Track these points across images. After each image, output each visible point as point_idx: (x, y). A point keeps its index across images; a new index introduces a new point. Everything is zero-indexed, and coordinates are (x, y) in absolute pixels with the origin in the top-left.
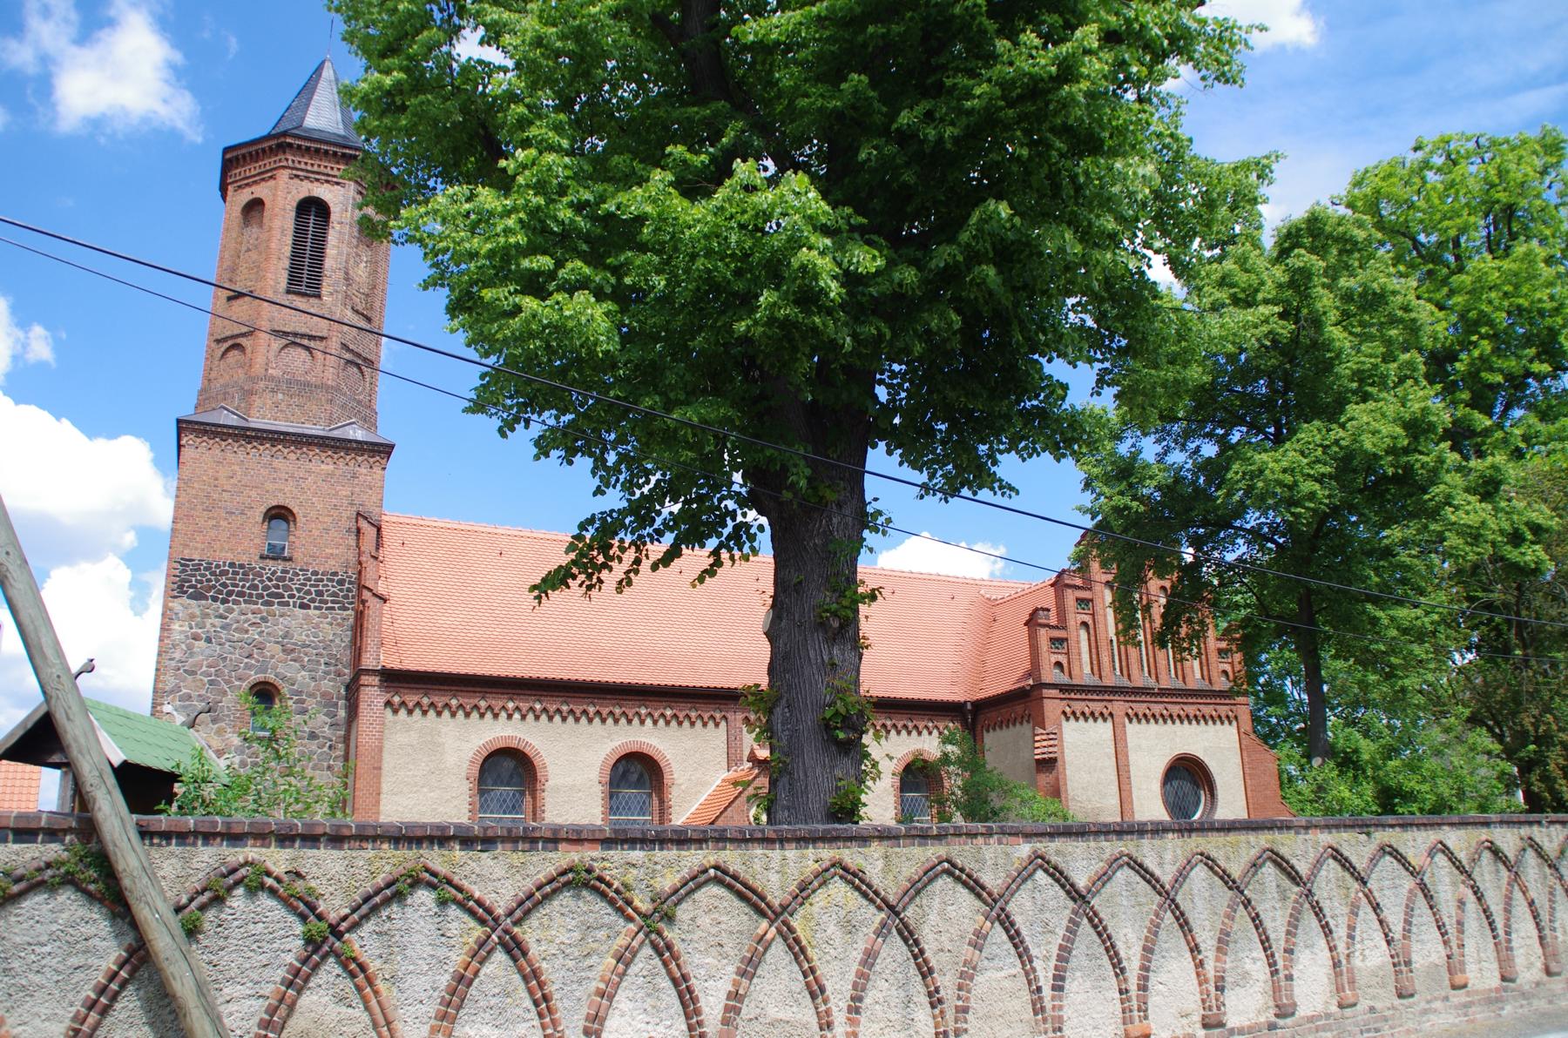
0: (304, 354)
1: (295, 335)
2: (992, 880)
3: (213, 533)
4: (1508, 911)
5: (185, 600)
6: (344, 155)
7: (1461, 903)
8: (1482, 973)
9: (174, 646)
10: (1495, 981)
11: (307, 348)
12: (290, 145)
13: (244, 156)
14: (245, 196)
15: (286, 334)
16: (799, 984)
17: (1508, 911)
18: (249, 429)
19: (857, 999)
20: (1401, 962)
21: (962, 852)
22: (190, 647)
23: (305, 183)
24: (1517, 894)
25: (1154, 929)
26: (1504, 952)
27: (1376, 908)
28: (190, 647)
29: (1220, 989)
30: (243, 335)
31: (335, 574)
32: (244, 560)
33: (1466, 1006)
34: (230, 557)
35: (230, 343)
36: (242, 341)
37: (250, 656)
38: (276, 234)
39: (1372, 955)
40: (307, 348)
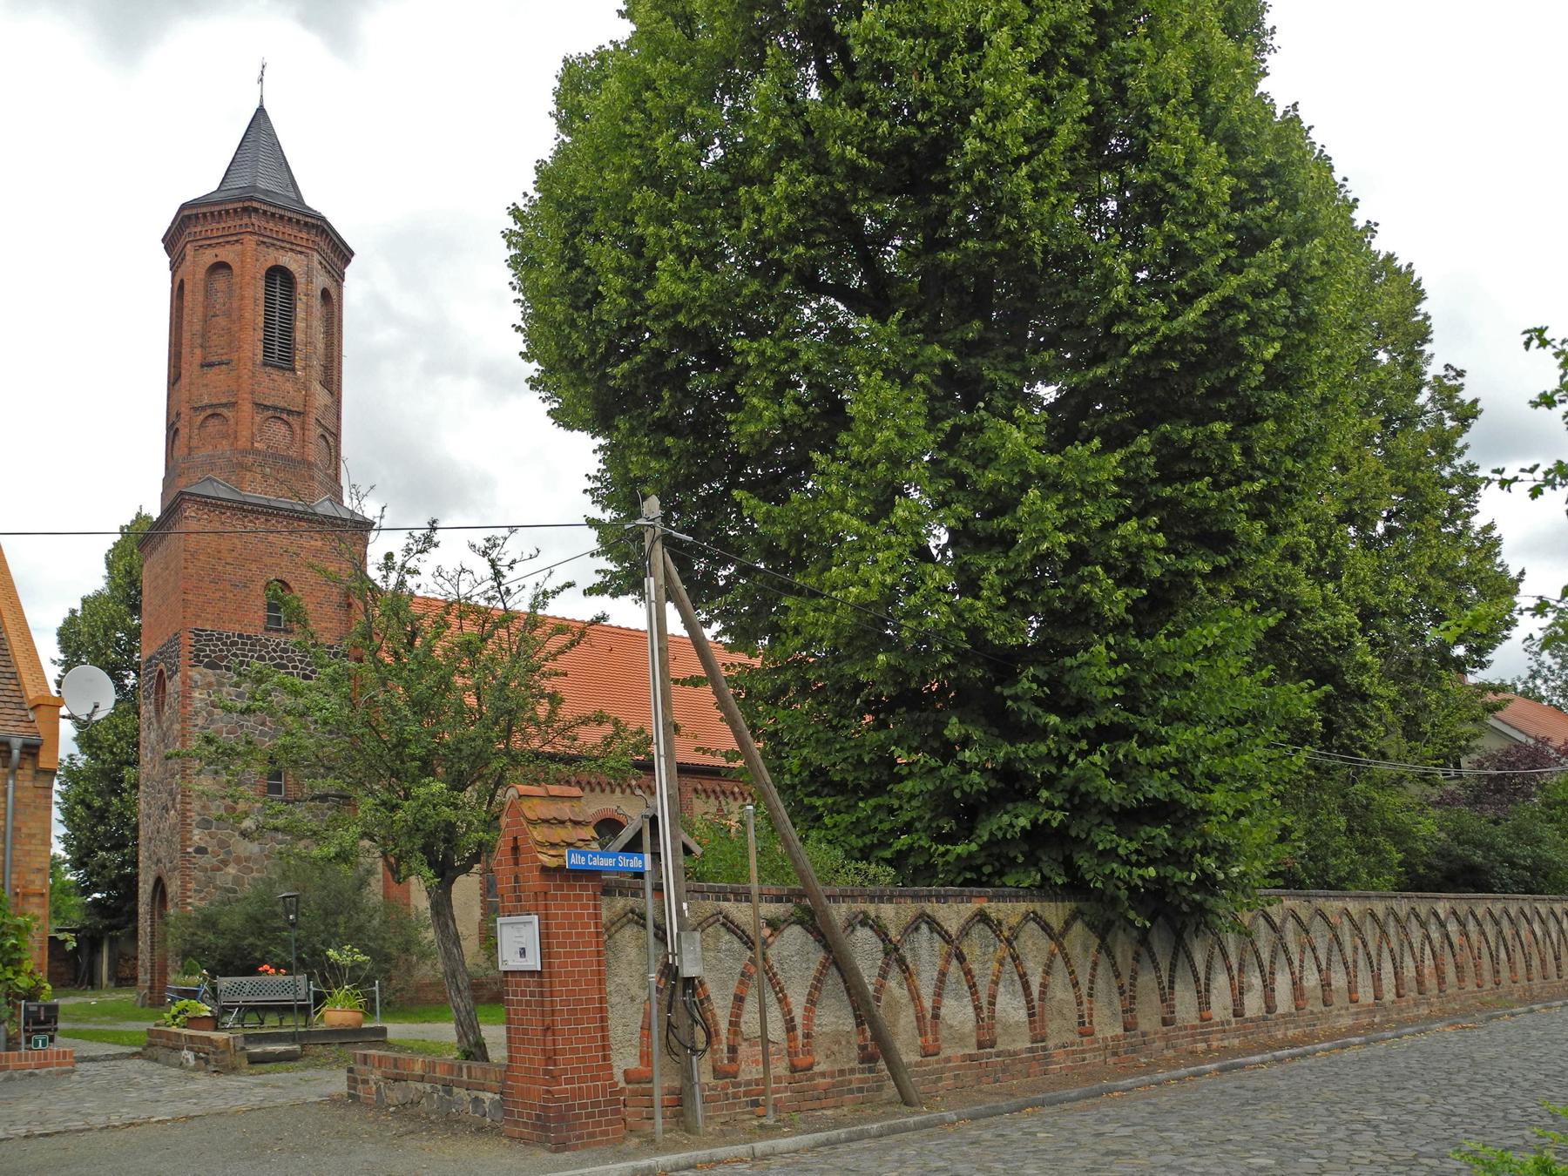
0: (284, 428)
1: (275, 408)
2: (953, 927)
3: (222, 604)
4: (1379, 955)
5: (201, 668)
6: (306, 224)
7: (1355, 949)
8: (1365, 995)
9: (196, 713)
10: (1371, 1000)
11: (287, 423)
12: (256, 210)
13: (204, 215)
14: (208, 257)
15: (267, 407)
16: (1067, 980)
17: (1379, 955)
18: (245, 503)
19: (1091, 989)
20: (1326, 984)
21: (995, 909)
22: (210, 714)
23: (271, 250)
24: (1384, 945)
25: (819, 981)
26: (1377, 979)
27: (1314, 950)
28: (210, 714)
29: (1241, 993)
30: (224, 405)
31: (331, 647)
32: (251, 631)
33: (1357, 1013)
34: (238, 628)
35: (209, 412)
37: (263, 724)
38: (248, 302)
39: (1311, 980)
40: (287, 423)
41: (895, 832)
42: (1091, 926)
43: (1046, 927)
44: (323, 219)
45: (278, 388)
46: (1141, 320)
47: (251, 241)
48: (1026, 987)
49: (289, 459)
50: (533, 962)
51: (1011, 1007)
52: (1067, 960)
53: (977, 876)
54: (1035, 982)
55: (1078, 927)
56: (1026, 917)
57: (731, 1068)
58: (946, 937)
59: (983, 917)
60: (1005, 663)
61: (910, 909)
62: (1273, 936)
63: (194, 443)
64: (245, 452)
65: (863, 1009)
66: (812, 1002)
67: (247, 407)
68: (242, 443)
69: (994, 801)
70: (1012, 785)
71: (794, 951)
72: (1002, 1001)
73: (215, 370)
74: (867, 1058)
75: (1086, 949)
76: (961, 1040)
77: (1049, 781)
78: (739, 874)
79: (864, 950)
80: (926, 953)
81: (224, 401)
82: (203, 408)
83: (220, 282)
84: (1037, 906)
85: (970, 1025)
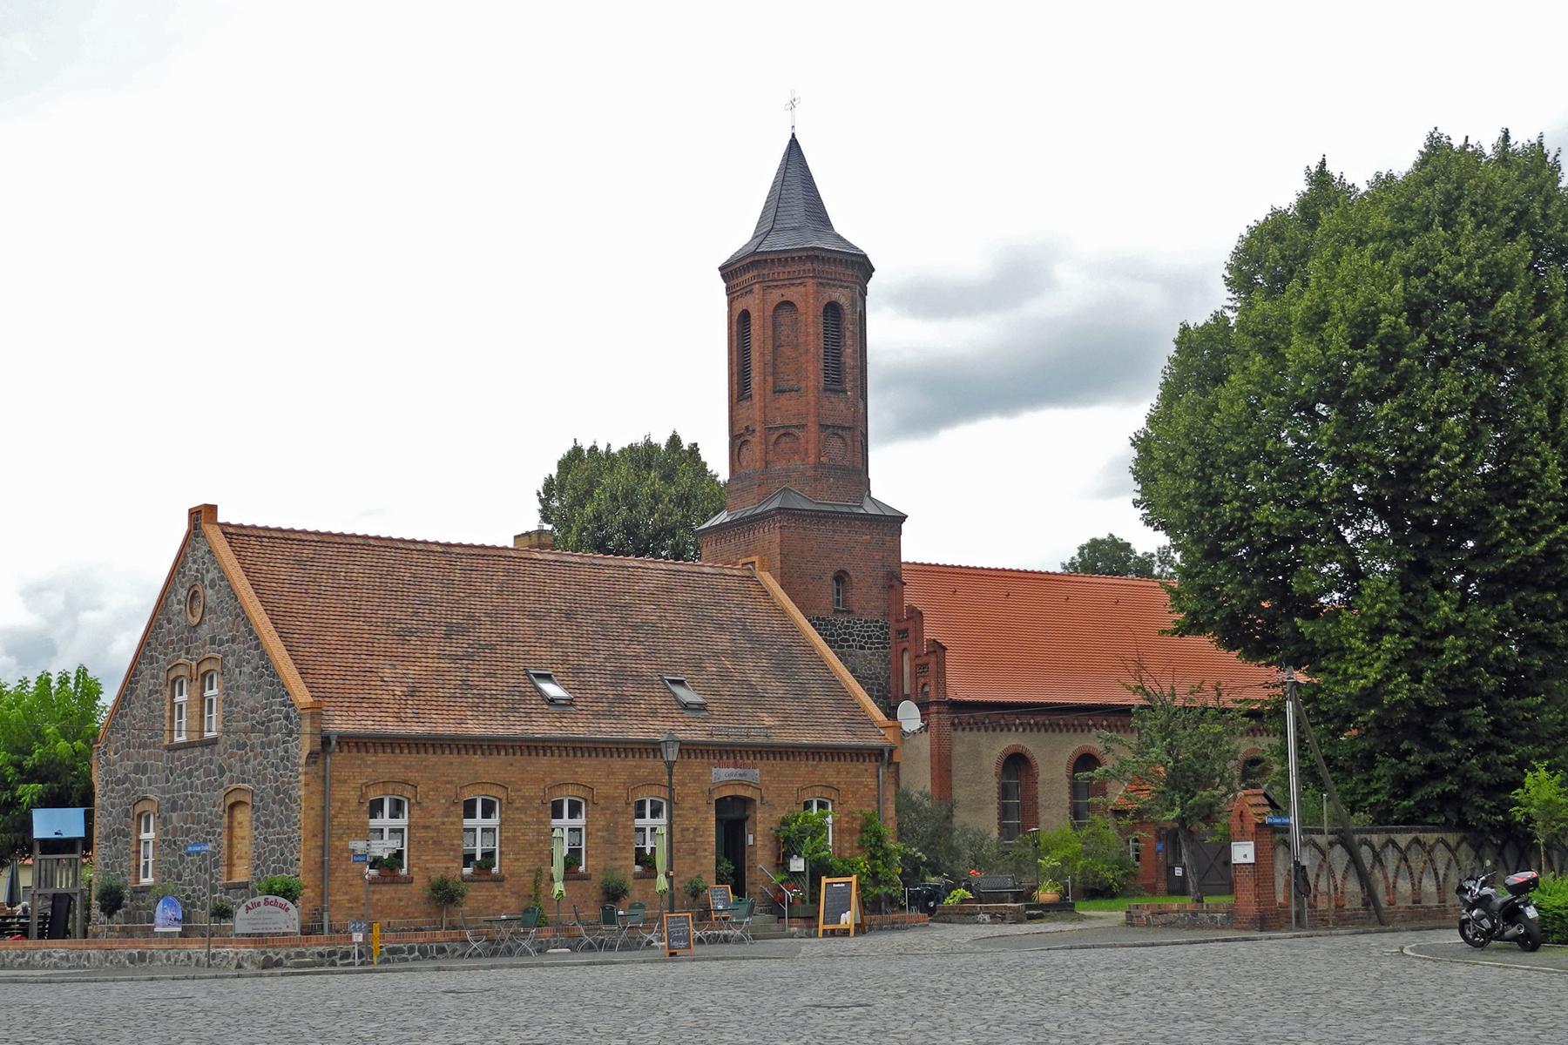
2: (1403, 846)
11: (841, 437)
14: (775, 296)
21: (1421, 836)
25: (1347, 868)
41: (1369, 794)
42: (1472, 846)
43: (1447, 846)
44: (865, 256)
46: (1513, 546)
48: (1436, 874)
50: (1251, 859)
51: (1429, 885)
52: (1458, 862)
53: (1410, 820)
54: (1441, 873)
55: (1464, 846)
56: (1438, 841)
58: (1399, 849)
59: (1417, 840)
60: (1430, 712)
61: (1383, 837)
63: (770, 457)
65: (1364, 879)
66: (1344, 878)
69: (1421, 781)
70: (1434, 771)
71: (1339, 856)
72: (1425, 881)
73: (787, 395)
74: (1366, 904)
75: (1468, 857)
76: (1405, 899)
77: (1452, 771)
78: (1319, 820)
79: (1366, 854)
80: (1391, 858)
83: (785, 318)
84: (1443, 835)
85: (1409, 893)
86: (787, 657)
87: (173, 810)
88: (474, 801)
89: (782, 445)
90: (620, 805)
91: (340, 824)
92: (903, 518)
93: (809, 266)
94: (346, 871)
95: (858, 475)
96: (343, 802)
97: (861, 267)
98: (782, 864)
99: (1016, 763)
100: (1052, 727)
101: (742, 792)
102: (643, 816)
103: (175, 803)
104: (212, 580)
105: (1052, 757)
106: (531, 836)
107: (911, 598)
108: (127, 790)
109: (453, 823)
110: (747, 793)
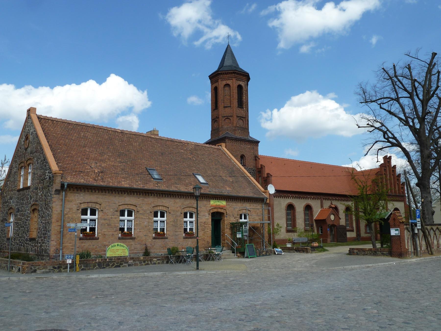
2: (435, 230)
14: (224, 82)
15: (239, 117)
36: (230, 118)
44: (248, 74)
45: (241, 112)
47: (234, 79)
49: (243, 128)
57: (261, 255)
62: (434, 233)
64: (235, 127)
67: (235, 117)
68: (235, 125)
73: (227, 108)
81: (229, 115)
82: (225, 117)
83: (227, 88)
86: (233, 172)
87: (18, 212)
88: (125, 211)
89: (226, 121)
90: (179, 214)
91: (68, 217)
92: (259, 142)
93: (233, 75)
94: (71, 235)
95: (246, 129)
96: (70, 209)
97: (246, 77)
98: (233, 234)
99: (291, 207)
100: (299, 198)
101: (220, 210)
102: (187, 218)
103: (18, 209)
104: (32, 132)
105: (300, 205)
106: (146, 223)
107: (261, 162)
108: (7, 205)
109: (115, 218)
110: (222, 211)
